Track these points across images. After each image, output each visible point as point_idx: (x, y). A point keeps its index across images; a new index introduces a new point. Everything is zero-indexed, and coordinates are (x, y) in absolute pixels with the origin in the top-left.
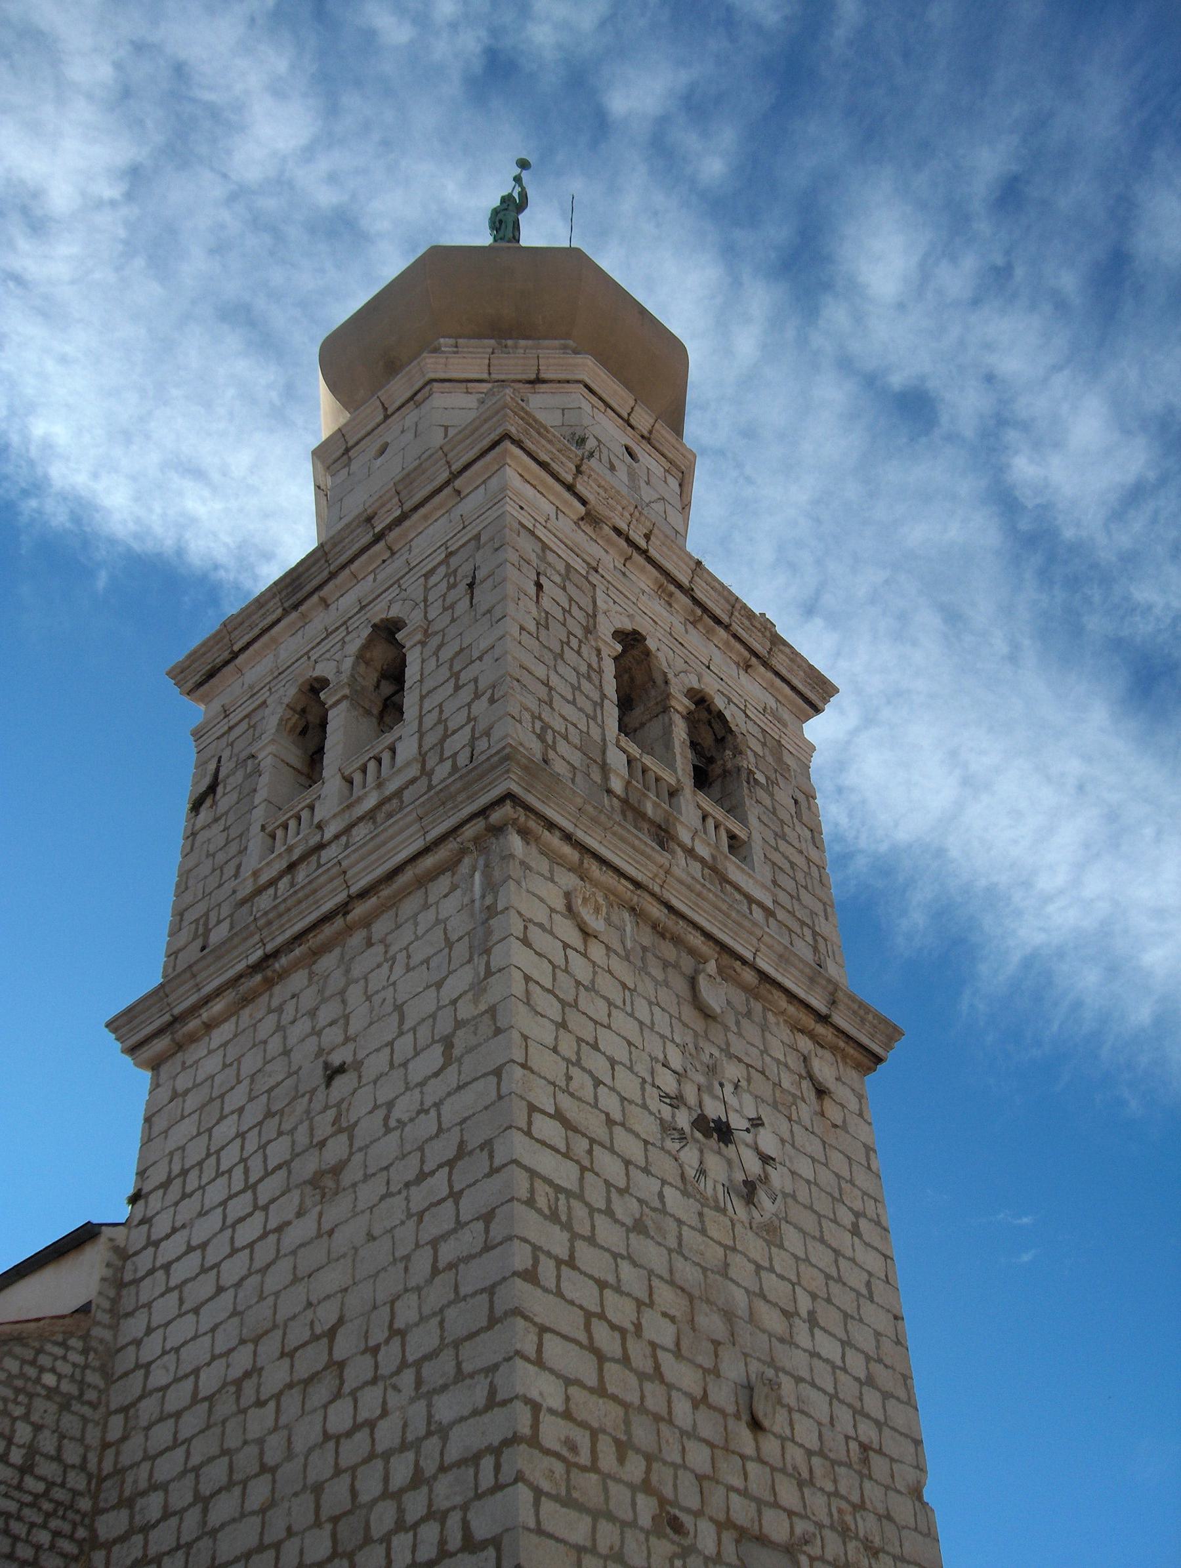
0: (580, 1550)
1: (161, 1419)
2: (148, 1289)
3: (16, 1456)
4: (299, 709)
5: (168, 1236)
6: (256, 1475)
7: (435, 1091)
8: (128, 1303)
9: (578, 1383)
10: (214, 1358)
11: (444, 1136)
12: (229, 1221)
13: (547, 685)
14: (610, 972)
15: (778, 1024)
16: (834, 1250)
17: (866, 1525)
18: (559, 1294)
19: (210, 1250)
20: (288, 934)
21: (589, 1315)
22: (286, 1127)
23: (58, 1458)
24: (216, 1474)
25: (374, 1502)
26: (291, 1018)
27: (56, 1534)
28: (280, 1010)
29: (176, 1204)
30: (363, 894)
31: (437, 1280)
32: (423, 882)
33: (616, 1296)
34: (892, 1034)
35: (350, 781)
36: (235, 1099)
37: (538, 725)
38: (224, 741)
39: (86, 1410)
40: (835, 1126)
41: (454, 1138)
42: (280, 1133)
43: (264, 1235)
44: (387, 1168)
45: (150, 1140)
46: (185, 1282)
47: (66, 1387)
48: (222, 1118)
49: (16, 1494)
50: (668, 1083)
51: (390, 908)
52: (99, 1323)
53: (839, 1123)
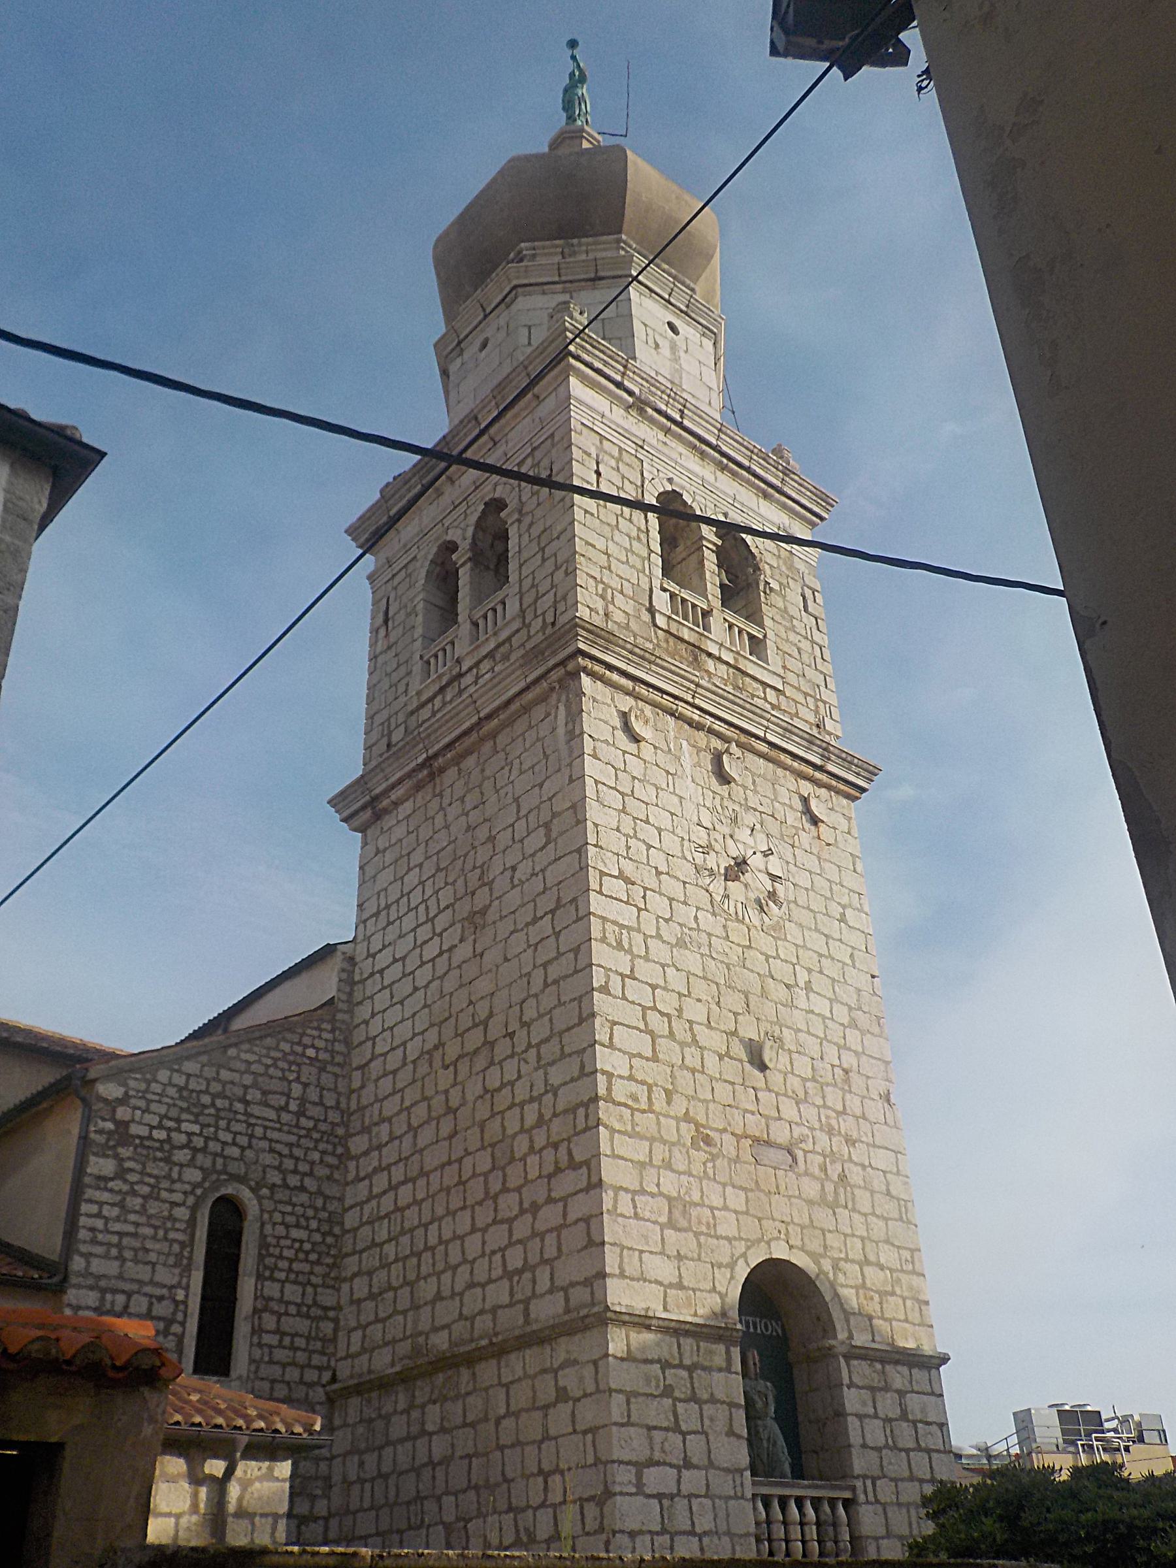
0: (642, 1165)
1: (385, 1075)
2: (371, 986)
3: (293, 1107)
4: (439, 561)
5: (380, 951)
6: (445, 1115)
7: (542, 859)
8: (358, 996)
9: (640, 1056)
10: (415, 1035)
11: (548, 892)
12: (419, 943)
13: (606, 554)
14: (657, 765)
15: (785, 777)
16: (826, 936)
17: (847, 1125)
18: (624, 998)
19: (408, 961)
20: (441, 744)
21: (644, 1009)
22: (450, 880)
23: (321, 1103)
24: (421, 1112)
25: (516, 1134)
26: (448, 801)
27: (323, 1152)
28: (441, 795)
29: (384, 929)
30: (489, 717)
31: (547, 990)
32: (526, 709)
33: (664, 993)
34: (872, 772)
35: (476, 625)
36: (417, 858)
37: (601, 586)
38: (389, 585)
39: (337, 1070)
40: (829, 845)
41: (552, 895)
42: (446, 884)
43: (441, 954)
44: (513, 912)
45: (364, 882)
46: (393, 983)
47: (323, 1056)
48: (410, 870)
49: (295, 1130)
50: (701, 836)
51: (507, 726)
52: (341, 1011)
53: (832, 841)
